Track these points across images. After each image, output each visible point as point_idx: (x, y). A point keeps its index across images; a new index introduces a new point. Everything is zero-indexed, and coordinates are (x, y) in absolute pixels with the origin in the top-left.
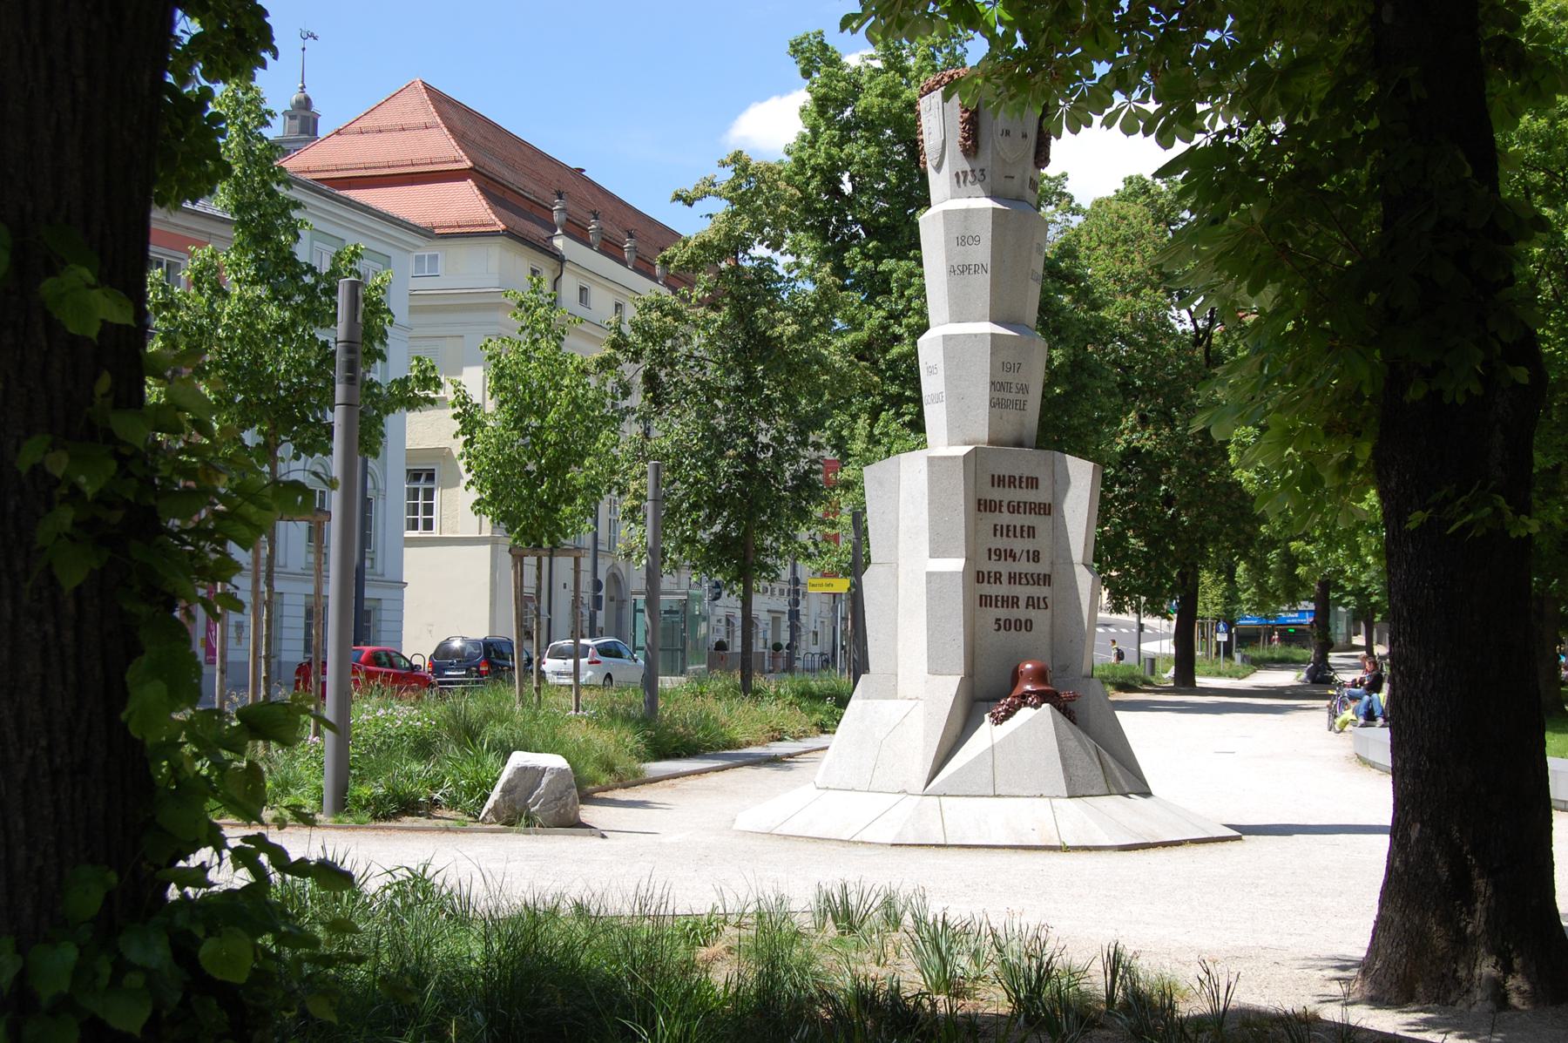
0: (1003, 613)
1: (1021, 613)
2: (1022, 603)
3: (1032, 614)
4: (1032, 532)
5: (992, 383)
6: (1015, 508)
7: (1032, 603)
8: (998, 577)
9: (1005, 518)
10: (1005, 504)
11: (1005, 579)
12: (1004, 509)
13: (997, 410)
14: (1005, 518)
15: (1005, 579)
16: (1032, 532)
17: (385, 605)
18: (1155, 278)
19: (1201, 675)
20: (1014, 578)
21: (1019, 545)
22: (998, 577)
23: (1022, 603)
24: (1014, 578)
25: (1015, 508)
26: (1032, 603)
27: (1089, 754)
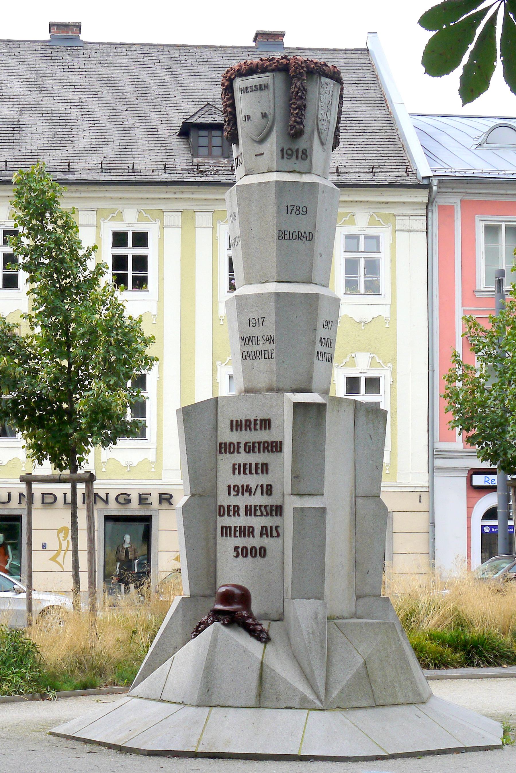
0: (241, 542)
1: (256, 542)
2: (257, 532)
3: (266, 542)
4: (265, 468)
5: (242, 339)
6: (250, 448)
7: (265, 532)
8: (236, 510)
9: (242, 458)
10: (242, 446)
11: (242, 511)
12: (242, 450)
13: (249, 362)
14: (242, 458)
15: (242, 511)
16: (265, 468)
17: (460, 608)
18: (78, 319)
19: (23, 611)
20: (250, 511)
21: (253, 481)
22: (236, 510)
23: (257, 532)
24: (250, 511)
25: (250, 448)
26: (265, 532)
27: (322, 647)
